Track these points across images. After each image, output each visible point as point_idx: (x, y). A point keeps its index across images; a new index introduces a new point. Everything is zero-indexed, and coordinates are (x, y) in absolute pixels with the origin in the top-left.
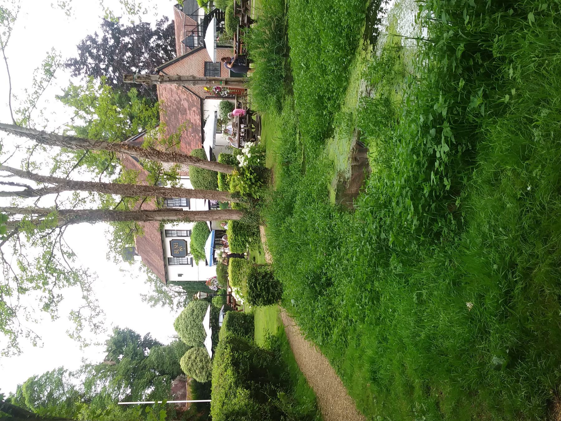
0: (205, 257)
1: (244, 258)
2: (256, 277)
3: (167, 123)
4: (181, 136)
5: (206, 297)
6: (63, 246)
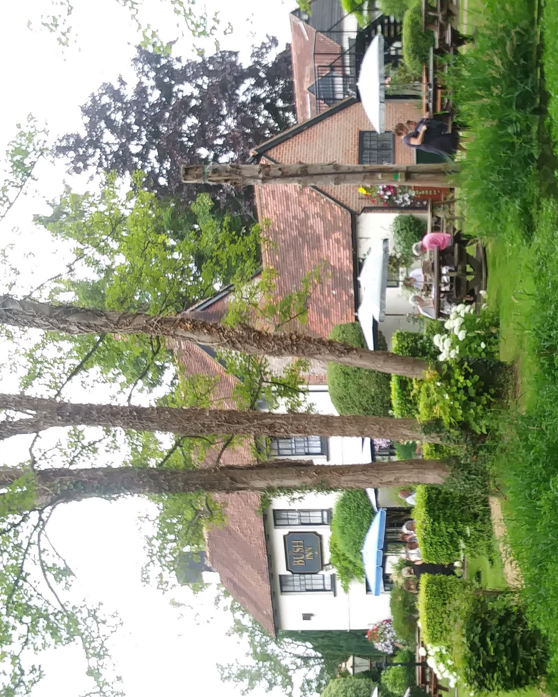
0: (362, 572)
1: (454, 574)
2: (484, 621)
3: (279, 269)
4: (309, 297)
5: (367, 668)
6: (46, 553)
